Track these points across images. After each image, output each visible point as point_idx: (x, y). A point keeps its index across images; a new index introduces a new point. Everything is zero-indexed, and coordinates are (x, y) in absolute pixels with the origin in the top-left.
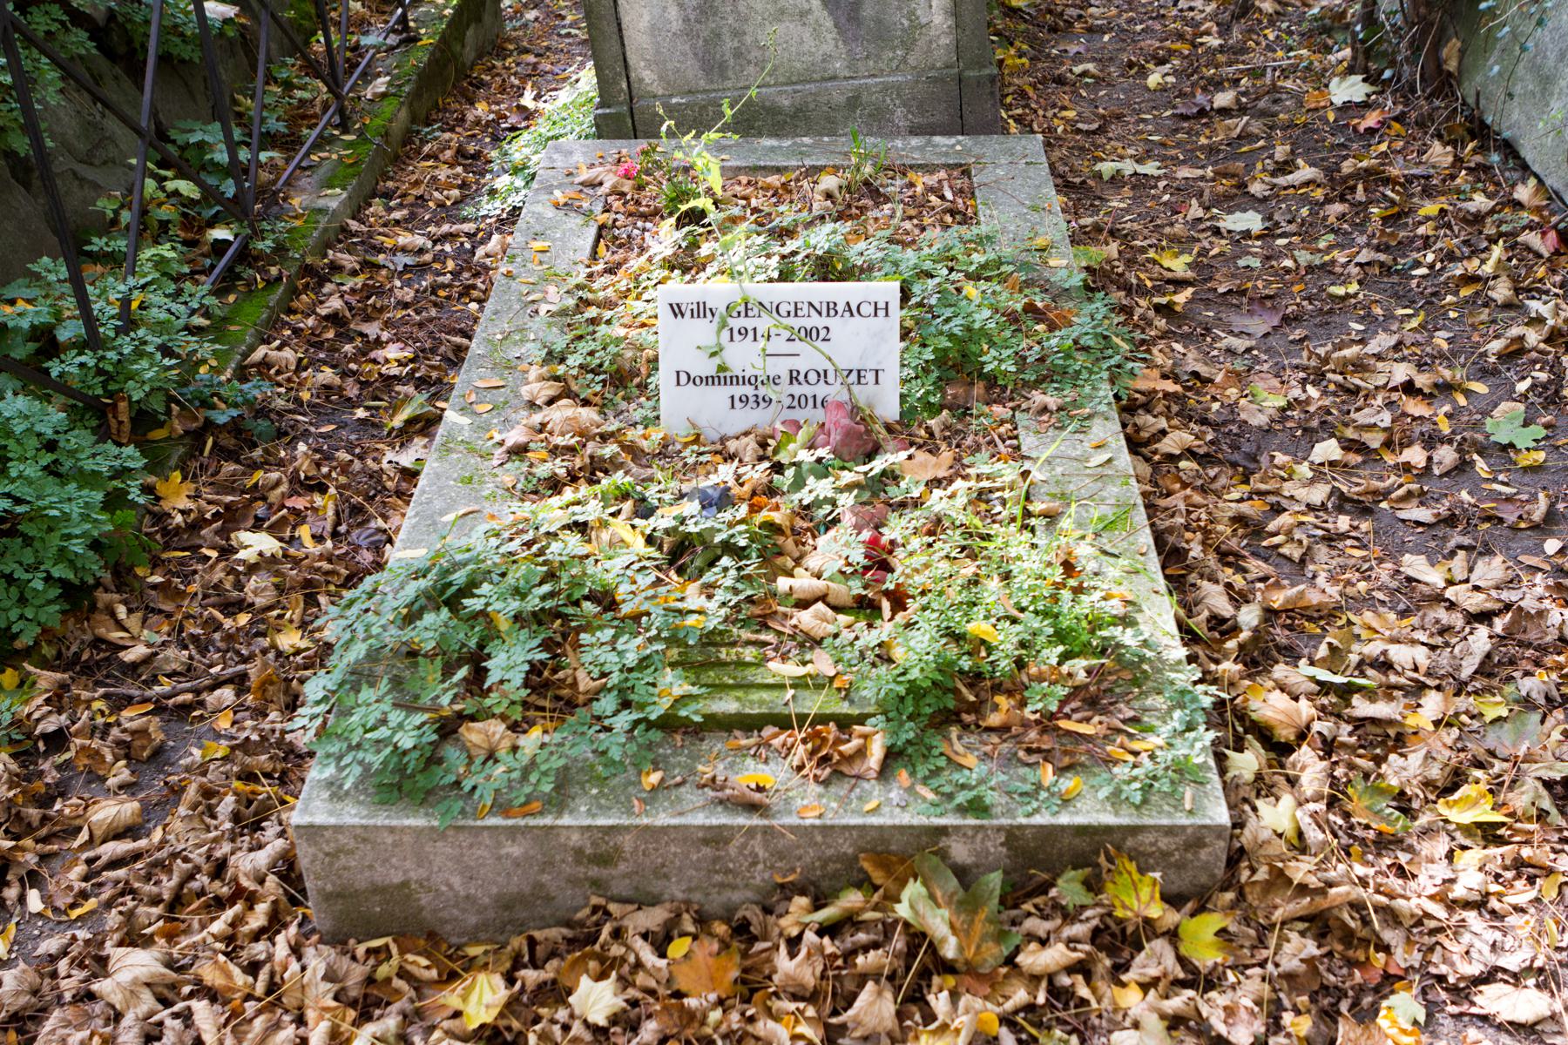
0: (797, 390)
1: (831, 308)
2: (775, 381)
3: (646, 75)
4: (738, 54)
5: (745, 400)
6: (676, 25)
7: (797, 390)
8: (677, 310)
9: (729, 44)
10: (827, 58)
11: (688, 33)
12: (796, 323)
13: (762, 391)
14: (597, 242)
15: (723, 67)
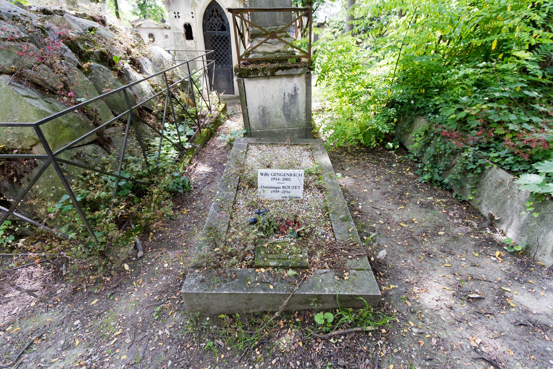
0: (284, 190)
1: (291, 175)
2: (280, 188)
3: (253, 126)
4: (269, 123)
5: (274, 191)
6: (258, 118)
7: (284, 190)
8: (262, 174)
9: (267, 121)
10: (284, 125)
11: (260, 120)
12: (284, 177)
13: (277, 190)
14: (272, 188)
15: (266, 125)
